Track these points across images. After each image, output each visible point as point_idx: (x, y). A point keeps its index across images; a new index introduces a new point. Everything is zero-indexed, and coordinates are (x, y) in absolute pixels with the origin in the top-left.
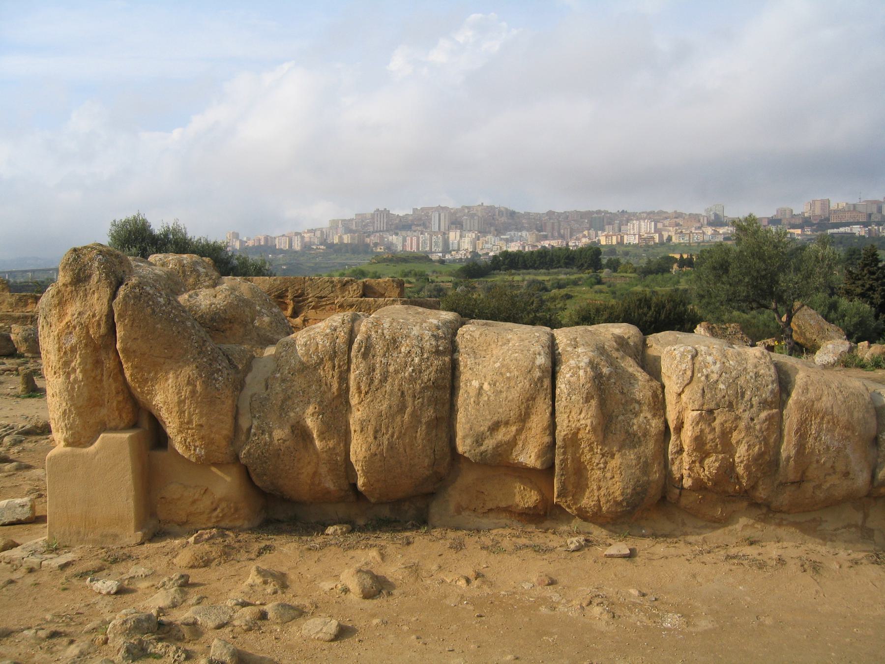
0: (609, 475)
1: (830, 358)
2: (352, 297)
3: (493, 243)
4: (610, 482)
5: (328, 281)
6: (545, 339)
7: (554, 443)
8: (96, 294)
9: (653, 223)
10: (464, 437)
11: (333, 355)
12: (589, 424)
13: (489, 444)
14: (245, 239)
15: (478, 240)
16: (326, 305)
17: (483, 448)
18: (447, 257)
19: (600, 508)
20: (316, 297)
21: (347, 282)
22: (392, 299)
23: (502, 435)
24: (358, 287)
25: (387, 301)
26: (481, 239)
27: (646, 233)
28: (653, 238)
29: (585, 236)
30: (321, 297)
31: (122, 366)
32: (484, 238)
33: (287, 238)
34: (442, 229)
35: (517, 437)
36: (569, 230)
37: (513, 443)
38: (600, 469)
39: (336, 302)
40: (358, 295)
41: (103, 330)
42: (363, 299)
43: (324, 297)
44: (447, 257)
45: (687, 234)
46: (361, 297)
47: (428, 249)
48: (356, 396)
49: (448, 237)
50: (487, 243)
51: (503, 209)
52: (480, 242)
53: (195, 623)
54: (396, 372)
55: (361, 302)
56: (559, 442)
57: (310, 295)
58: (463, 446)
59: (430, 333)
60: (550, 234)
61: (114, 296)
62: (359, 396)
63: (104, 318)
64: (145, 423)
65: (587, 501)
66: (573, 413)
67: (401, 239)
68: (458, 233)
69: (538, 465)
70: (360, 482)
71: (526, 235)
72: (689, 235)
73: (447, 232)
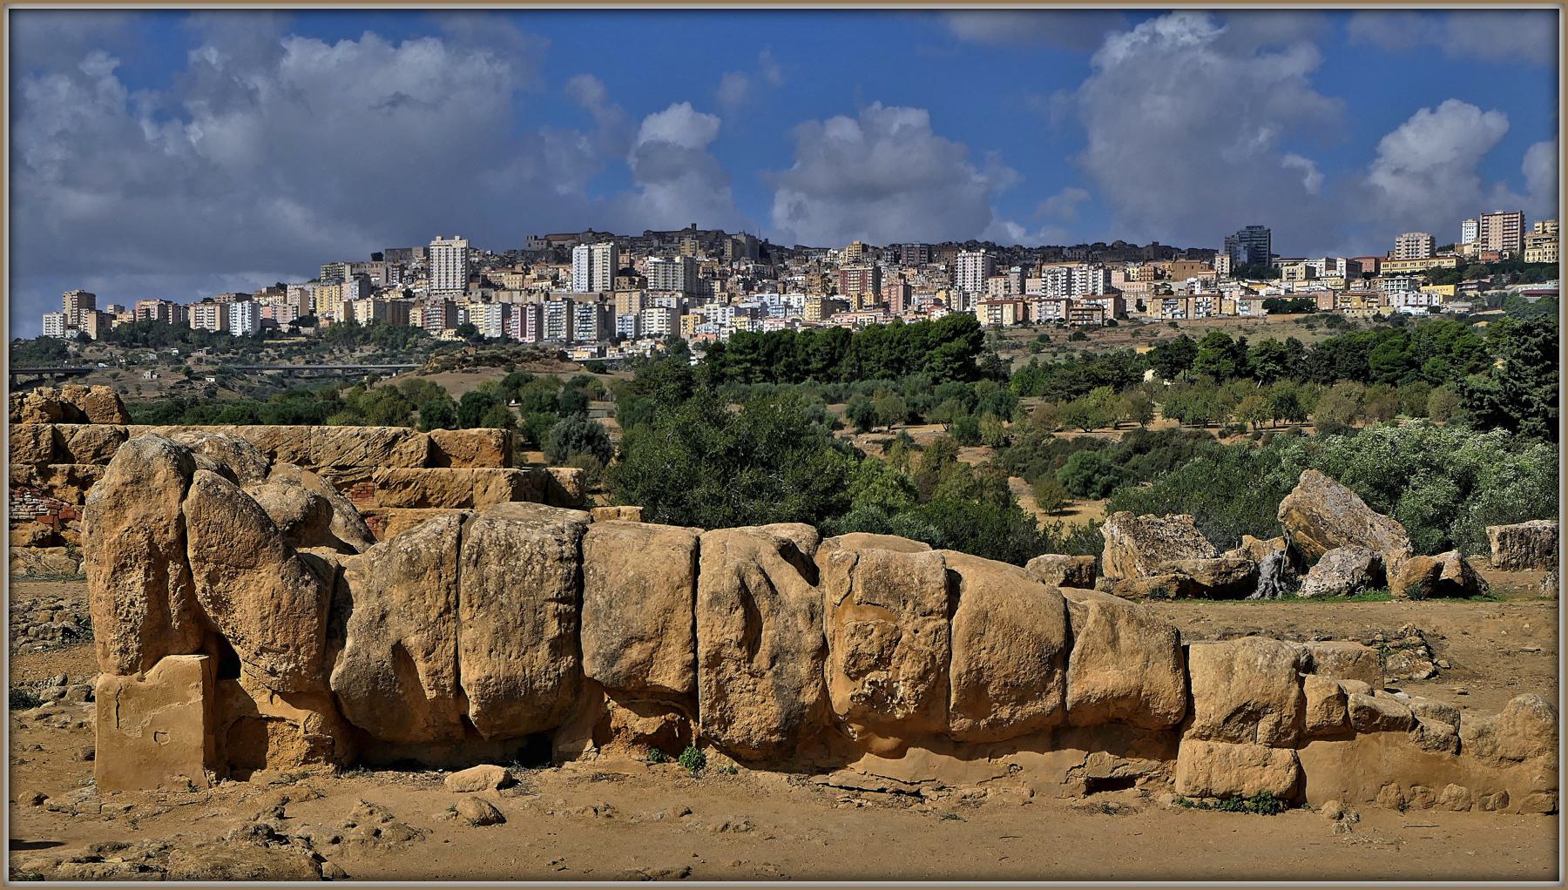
0: (759, 698)
1: (1334, 582)
2: (407, 466)
3: (719, 321)
4: (762, 707)
5: (358, 435)
6: (690, 543)
7: (696, 660)
8: (163, 495)
9: (1101, 272)
10: (593, 658)
11: (440, 562)
12: (734, 639)
13: (622, 665)
14: (110, 309)
15: (686, 313)
16: (354, 482)
17: (615, 669)
18: (609, 356)
19: (750, 740)
20: (333, 467)
21: (396, 437)
22: (487, 469)
23: (635, 653)
24: (418, 447)
25: (478, 474)
26: (691, 311)
27: (1084, 297)
28: (1100, 308)
29: (938, 303)
30: (344, 467)
31: (191, 576)
32: (699, 310)
33: (218, 308)
34: (598, 289)
35: (654, 656)
36: (901, 288)
37: (648, 662)
38: (749, 691)
39: (375, 476)
40: (419, 462)
41: (171, 536)
42: (429, 470)
43: (350, 467)
44: (609, 356)
45: (1182, 298)
46: (426, 467)
47: (563, 335)
48: (468, 609)
49: (612, 307)
50: (705, 319)
51: (743, 239)
52: (690, 318)
53: (308, 839)
54: (514, 582)
55: (426, 476)
56: (702, 662)
57: (323, 464)
58: (590, 668)
59: (553, 537)
60: (854, 301)
61: (184, 496)
62: (471, 611)
63: (173, 523)
64: (213, 647)
65: (735, 733)
66: (716, 627)
67: (497, 311)
68: (636, 296)
69: (677, 686)
70: (473, 710)
71: (799, 301)
72: (1188, 301)
73: (609, 295)
